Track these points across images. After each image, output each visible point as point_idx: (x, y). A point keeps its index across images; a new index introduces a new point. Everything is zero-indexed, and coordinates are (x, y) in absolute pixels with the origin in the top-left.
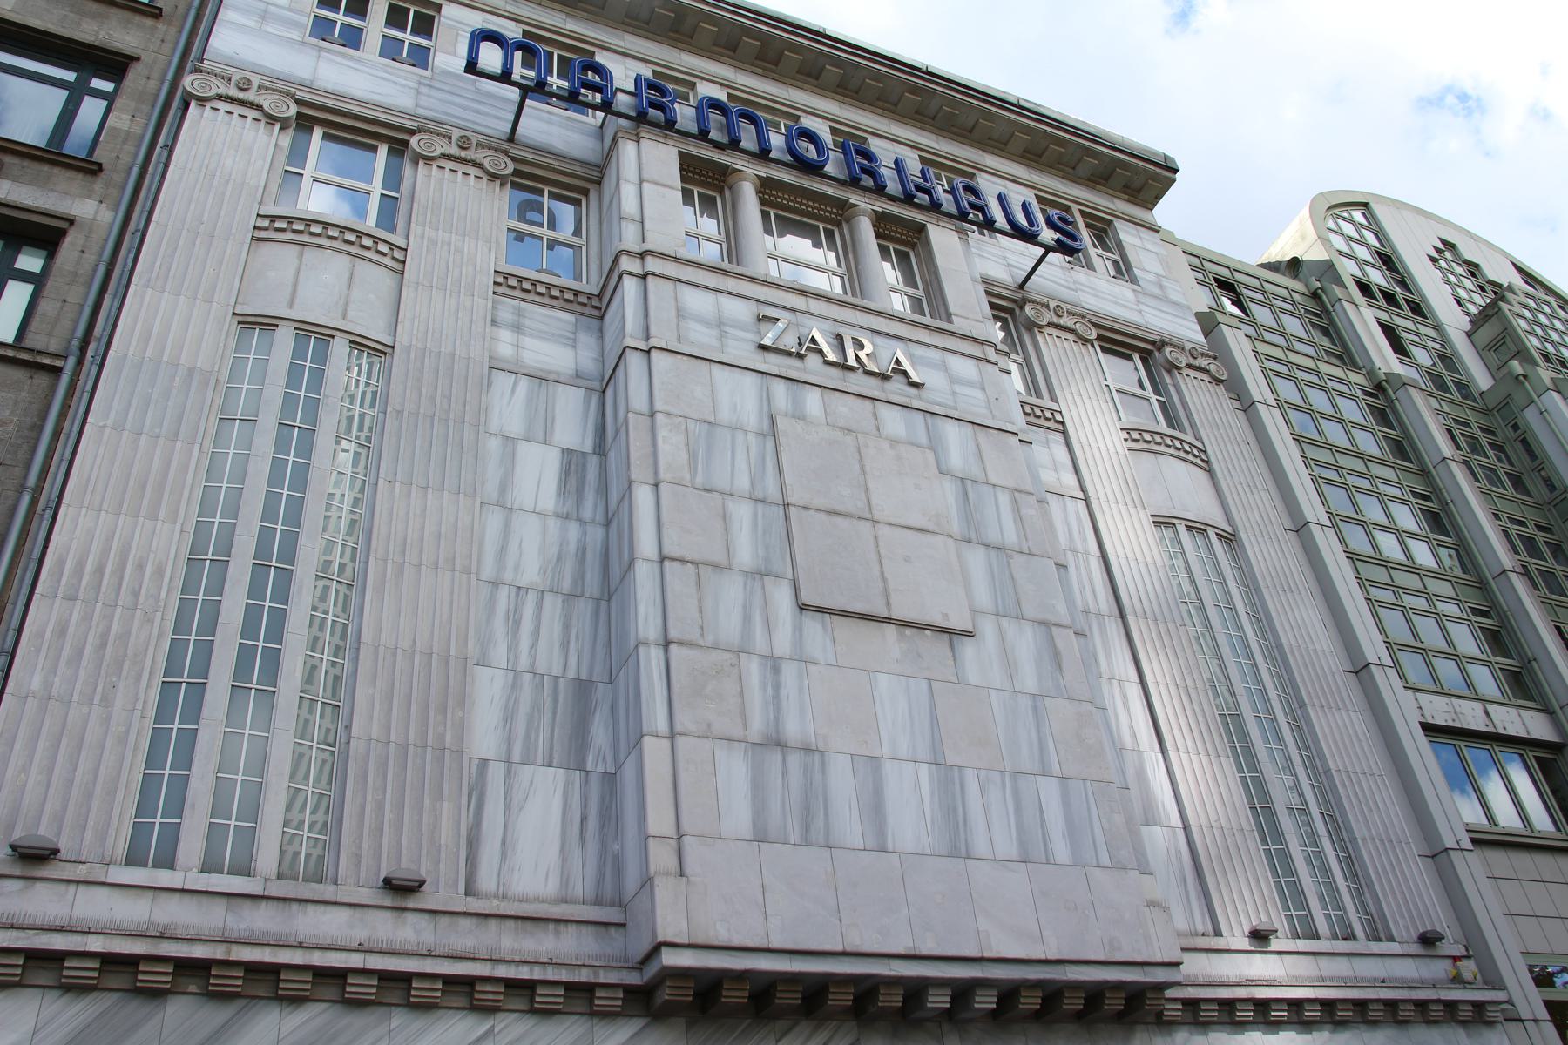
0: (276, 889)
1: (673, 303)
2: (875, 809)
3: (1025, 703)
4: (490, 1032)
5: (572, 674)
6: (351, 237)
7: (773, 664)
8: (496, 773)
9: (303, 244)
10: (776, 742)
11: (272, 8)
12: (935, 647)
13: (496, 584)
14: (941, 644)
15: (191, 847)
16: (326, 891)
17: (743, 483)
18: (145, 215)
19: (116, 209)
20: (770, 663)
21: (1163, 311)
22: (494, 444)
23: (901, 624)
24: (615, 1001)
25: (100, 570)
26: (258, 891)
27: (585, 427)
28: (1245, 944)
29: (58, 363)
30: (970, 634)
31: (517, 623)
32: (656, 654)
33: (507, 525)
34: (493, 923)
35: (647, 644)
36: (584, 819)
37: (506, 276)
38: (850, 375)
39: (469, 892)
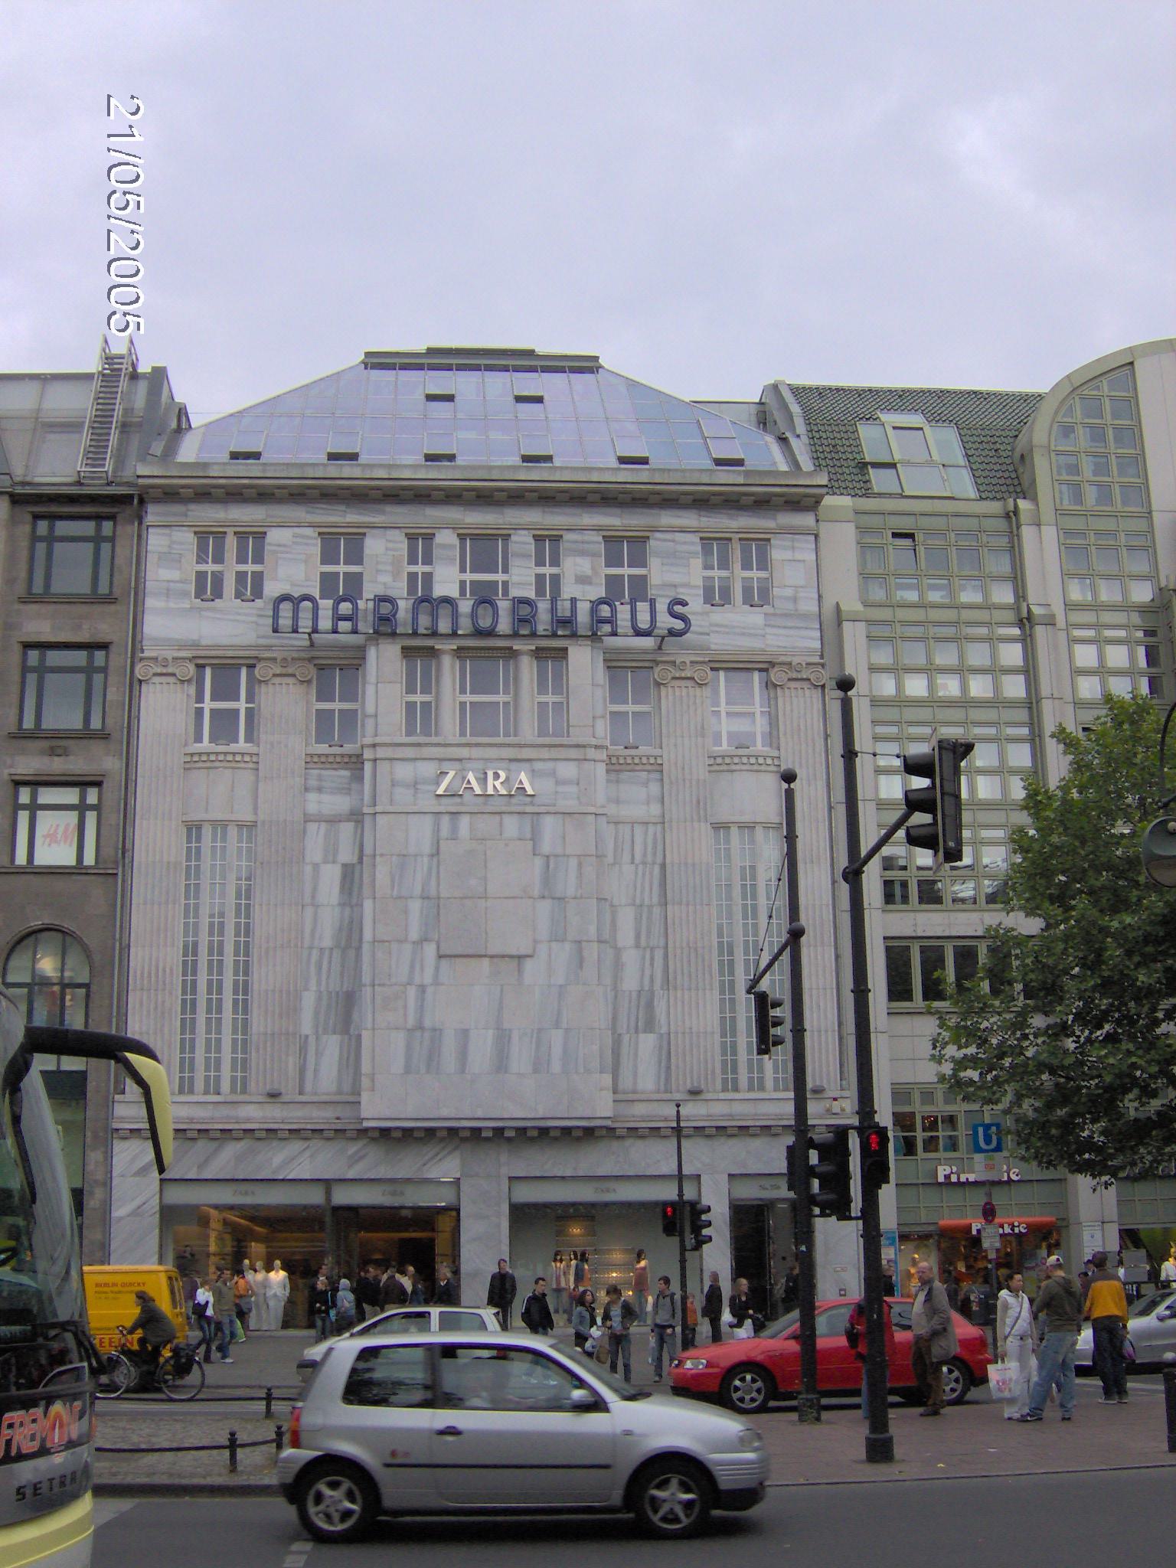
5: (345, 989)
8: (312, 1040)
13: (311, 948)
15: (199, 1085)
17: (418, 890)
21: (791, 628)
24: (354, 1134)
25: (150, 974)
32: (369, 989)
33: (316, 914)
37: (312, 756)
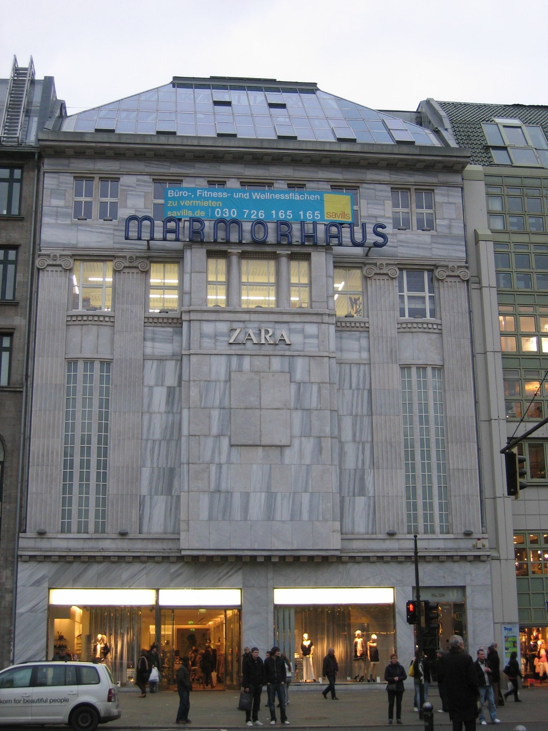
0: (94, 536)
1: (199, 331)
2: (246, 509)
3: (304, 468)
4: (145, 567)
5: (169, 466)
6: (96, 319)
7: (220, 465)
8: (148, 499)
9: (82, 325)
10: (218, 491)
11: (59, 209)
12: (276, 453)
14: (277, 451)
15: (74, 527)
16: (105, 536)
17: (217, 403)
18: (33, 341)
19: (25, 318)
20: (219, 466)
22: (146, 390)
23: (264, 446)
25: (43, 456)
26: (90, 537)
27: (175, 376)
28: (386, 537)
29: (21, 390)
30: (288, 446)
31: (153, 452)
34: (145, 541)
35: (183, 464)
36: (171, 509)
38: (263, 346)
39: (140, 533)
